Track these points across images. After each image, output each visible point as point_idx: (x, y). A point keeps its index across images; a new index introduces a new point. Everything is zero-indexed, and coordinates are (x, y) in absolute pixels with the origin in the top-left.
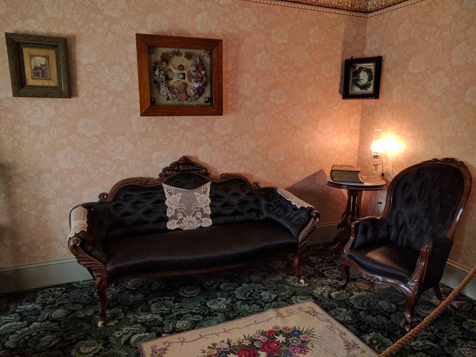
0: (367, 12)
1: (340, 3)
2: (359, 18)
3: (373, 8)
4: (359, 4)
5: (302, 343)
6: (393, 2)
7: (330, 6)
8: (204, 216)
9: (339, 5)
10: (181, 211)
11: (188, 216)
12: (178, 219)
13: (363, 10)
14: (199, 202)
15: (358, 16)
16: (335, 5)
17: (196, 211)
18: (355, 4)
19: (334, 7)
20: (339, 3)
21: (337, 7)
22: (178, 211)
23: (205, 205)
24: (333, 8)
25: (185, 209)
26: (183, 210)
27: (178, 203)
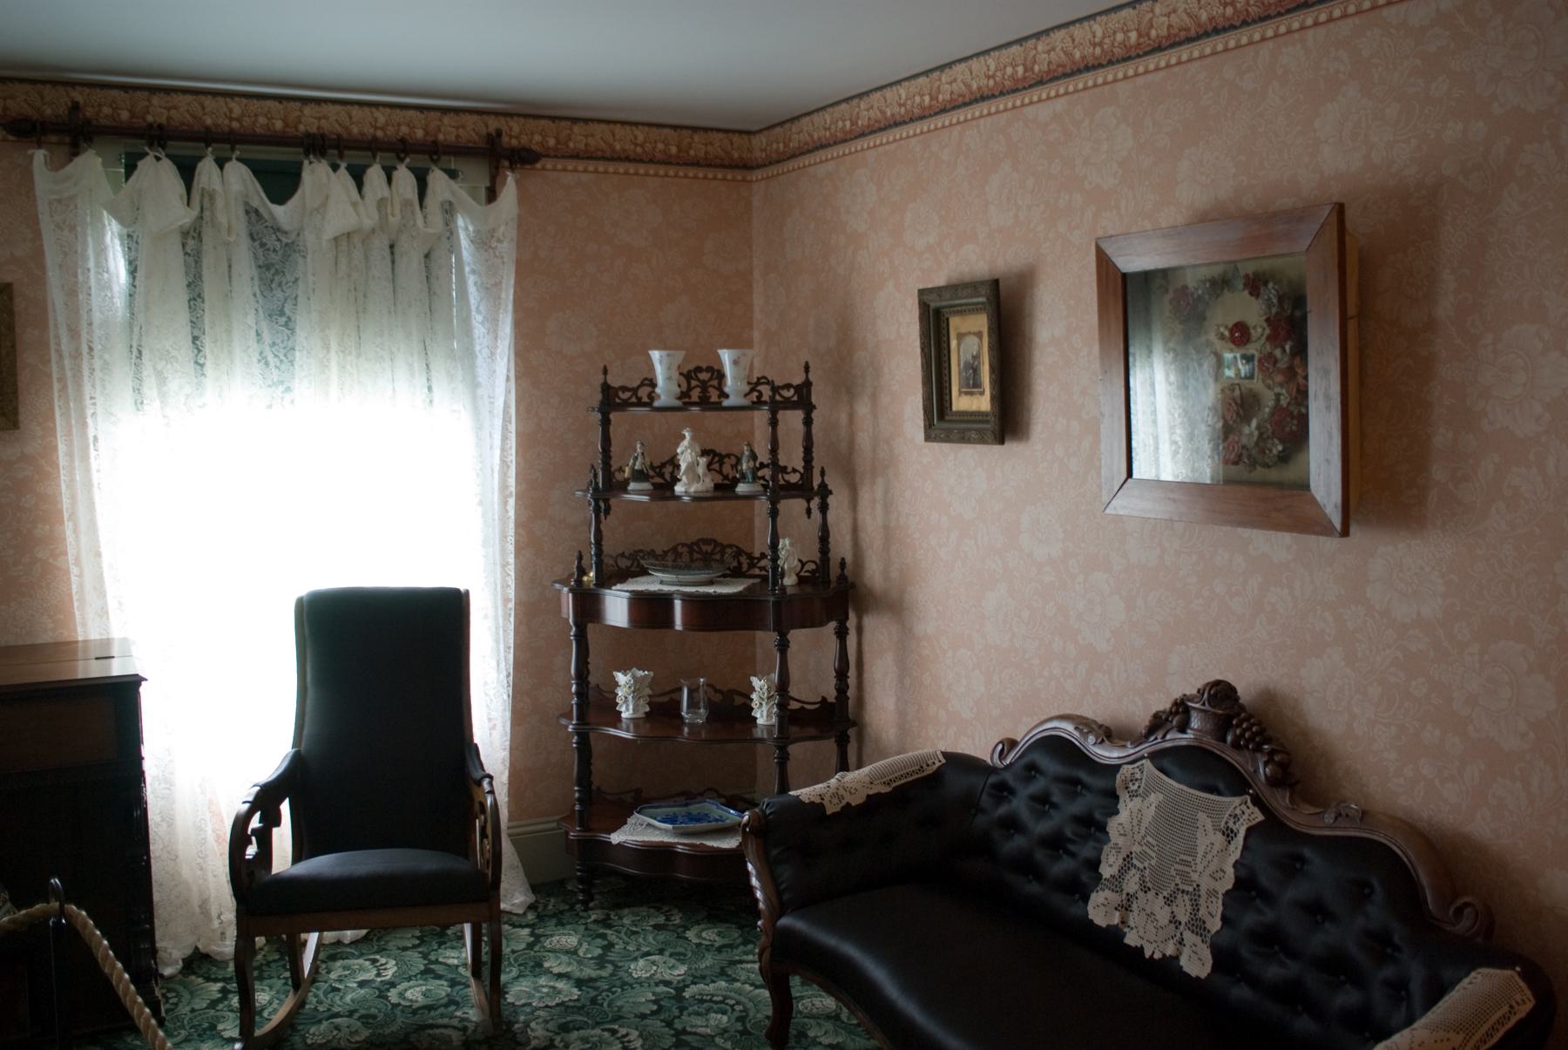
0: (747, 166)
1: (642, 146)
2: (1140, 81)
3: (1224, 15)
4: (706, 145)
5: (697, 947)
6: (1169, 36)
7: (608, 154)
8: (1198, 926)
9: (639, 150)
10: (1141, 866)
11: (1153, 892)
12: (1125, 892)
13: (1183, 34)
14: (1198, 860)
15: (1136, 75)
16: (625, 151)
17: (1181, 887)
18: (690, 144)
19: (623, 156)
20: (636, 145)
21: (632, 157)
22: (1135, 861)
23: (1213, 884)
24: (620, 159)
25: (1153, 862)
26: (1146, 865)
27: (1143, 832)
